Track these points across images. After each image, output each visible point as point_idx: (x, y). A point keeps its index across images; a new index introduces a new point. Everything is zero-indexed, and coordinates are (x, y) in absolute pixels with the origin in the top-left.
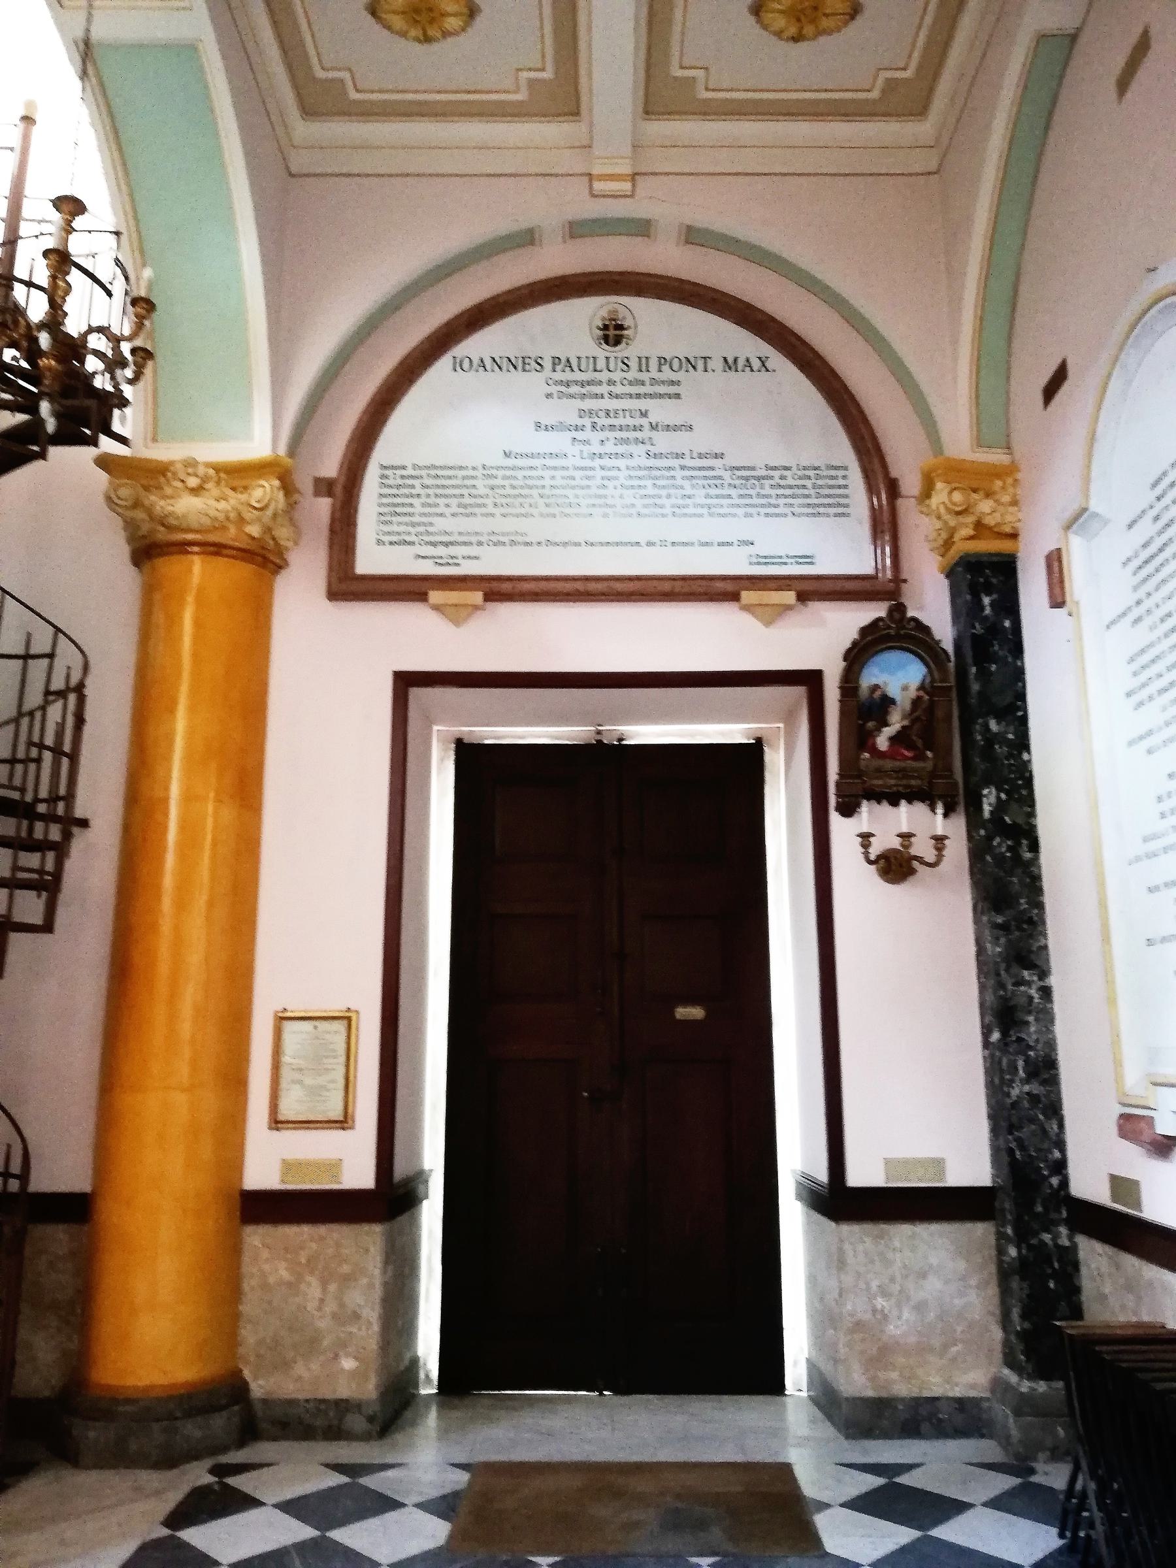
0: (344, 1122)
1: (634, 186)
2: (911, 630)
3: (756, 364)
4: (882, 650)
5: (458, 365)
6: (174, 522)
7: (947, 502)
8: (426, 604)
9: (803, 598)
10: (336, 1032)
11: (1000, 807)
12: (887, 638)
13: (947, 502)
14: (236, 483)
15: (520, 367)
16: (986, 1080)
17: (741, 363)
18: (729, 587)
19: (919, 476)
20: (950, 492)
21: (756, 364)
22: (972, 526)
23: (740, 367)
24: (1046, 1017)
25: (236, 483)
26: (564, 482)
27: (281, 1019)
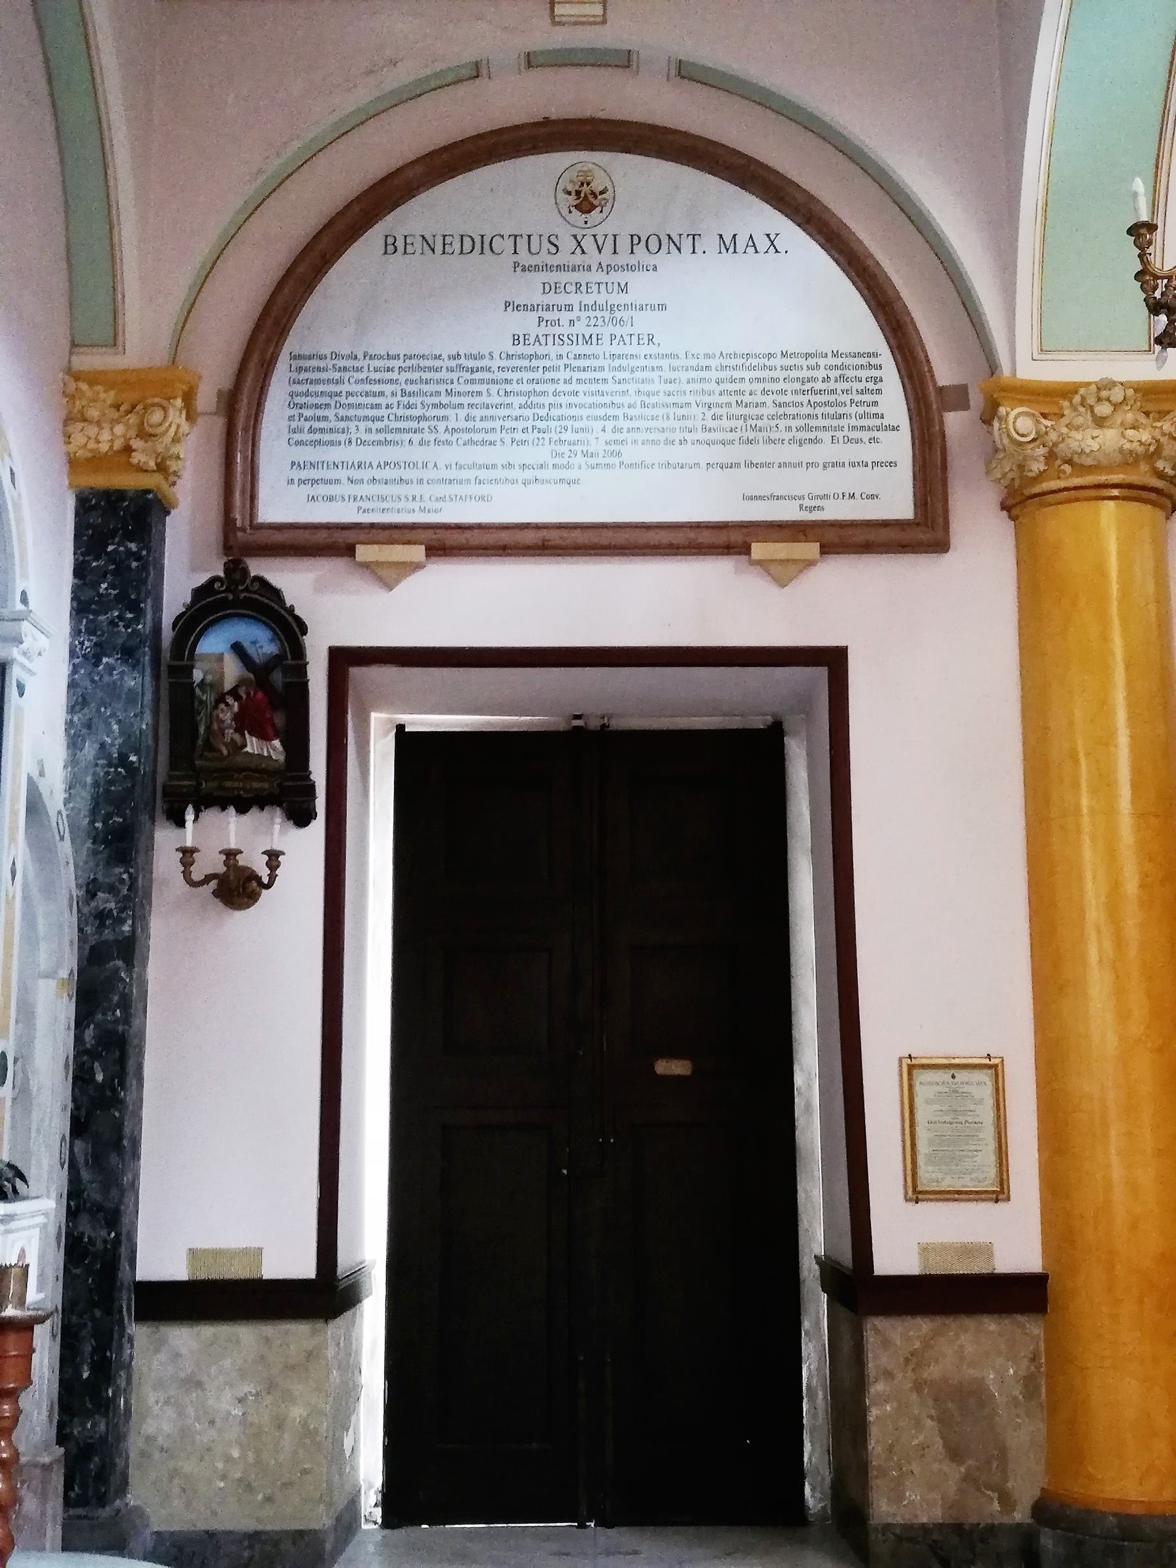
0: (1000, 1194)
1: (605, 9)
2: (255, 592)
3: (762, 244)
4: (264, 623)
5: (390, 246)
6: (1089, 462)
8: (744, 558)
9: (827, 549)
10: (979, 1084)
12: (222, 604)
14: (1151, 407)
15: (439, 248)
17: (741, 242)
18: (736, 537)
21: (762, 244)
22: (1042, 459)
23: (740, 249)
25: (1151, 407)
26: (590, 400)
27: (912, 1068)
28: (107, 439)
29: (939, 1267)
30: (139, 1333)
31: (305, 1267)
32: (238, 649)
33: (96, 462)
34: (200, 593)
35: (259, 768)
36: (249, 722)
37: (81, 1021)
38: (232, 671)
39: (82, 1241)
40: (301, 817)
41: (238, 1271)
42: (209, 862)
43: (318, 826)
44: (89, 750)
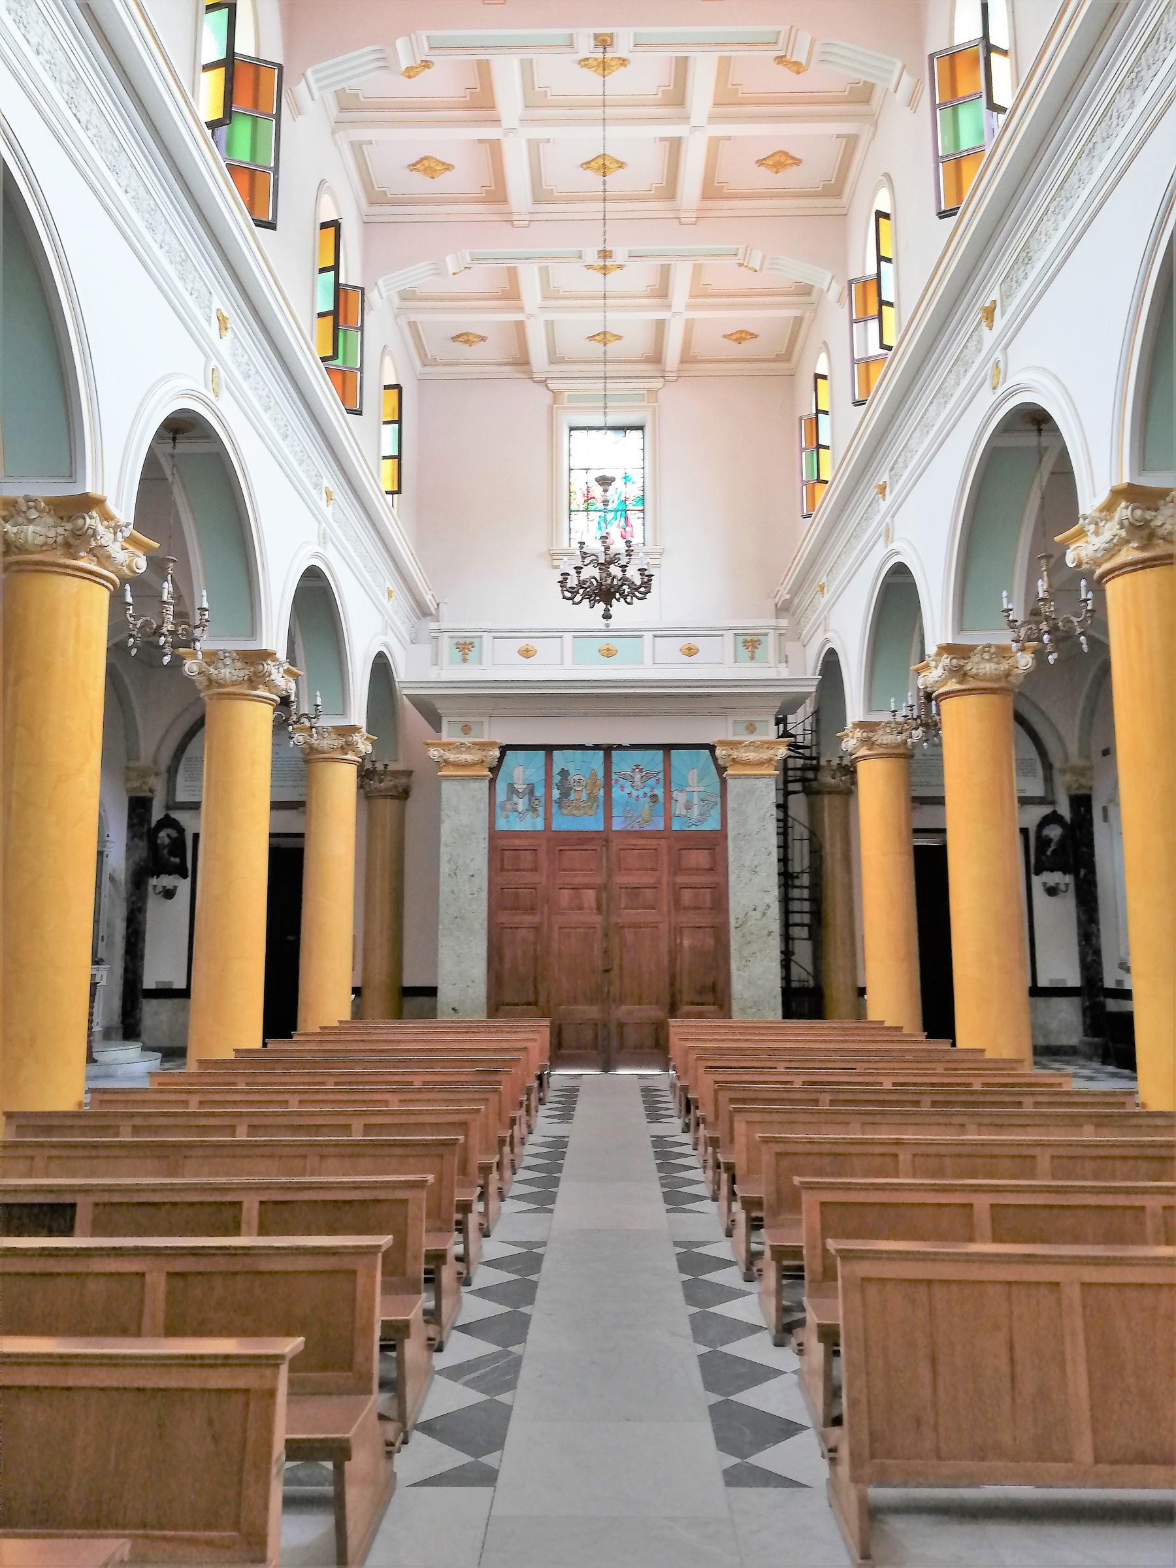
7: (1130, 517)
11: (1085, 875)
13: (1130, 517)
16: (1084, 1023)
19: (529, 1337)
20: (1133, 510)
24: (1098, 937)
28: (136, 784)
29: (160, 987)
30: (144, 1001)
31: (183, 985)
32: (168, 836)
33: (133, 790)
34: (159, 822)
35: (174, 864)
36: (171, 853)
37: (128, 927)
38: (167, 841)
39: (794, 1175)
40: (185, 877)
41: (167, 987)
42: (159, 889)
43: (189, 879)
44: (131, 862)
